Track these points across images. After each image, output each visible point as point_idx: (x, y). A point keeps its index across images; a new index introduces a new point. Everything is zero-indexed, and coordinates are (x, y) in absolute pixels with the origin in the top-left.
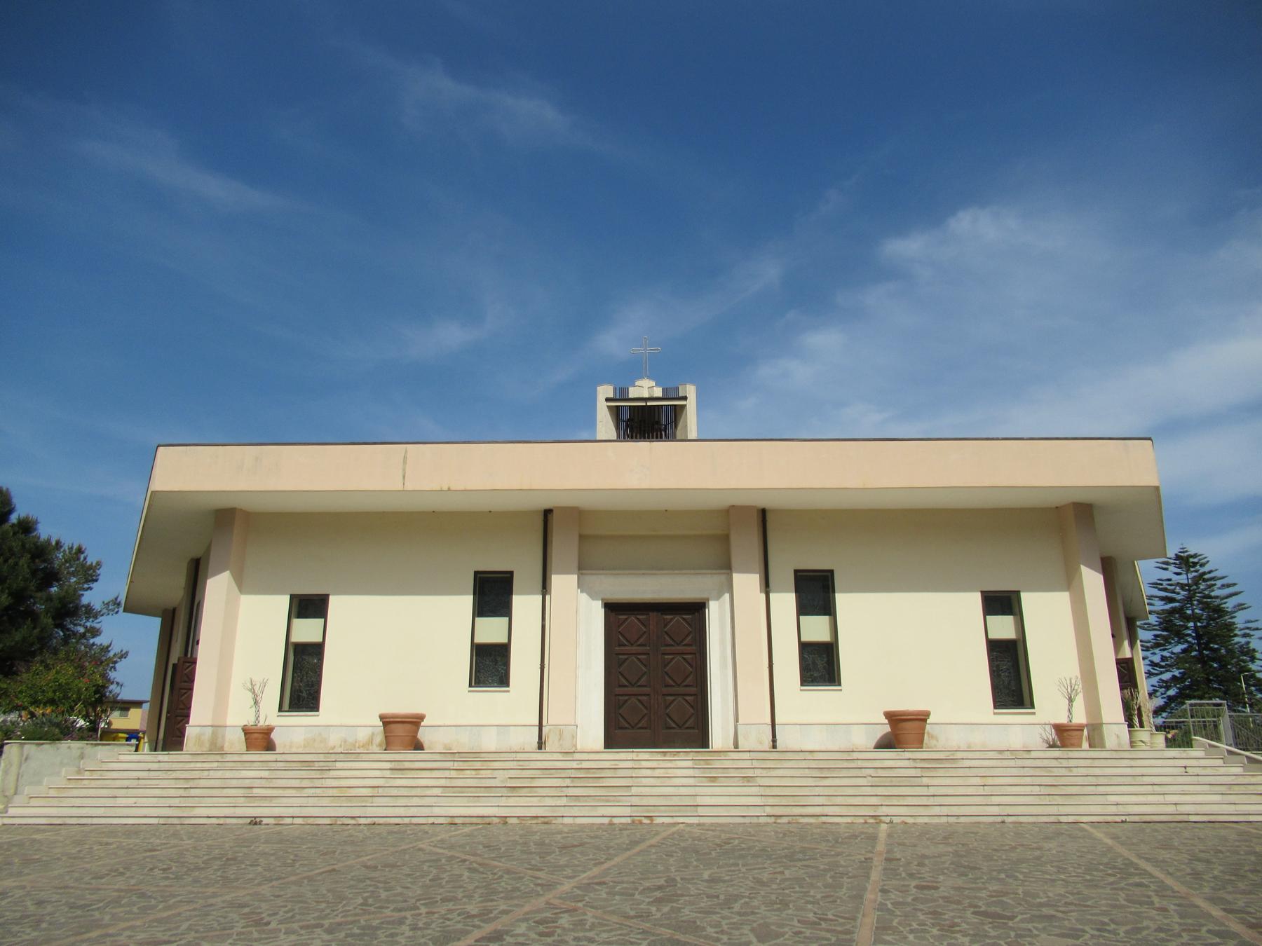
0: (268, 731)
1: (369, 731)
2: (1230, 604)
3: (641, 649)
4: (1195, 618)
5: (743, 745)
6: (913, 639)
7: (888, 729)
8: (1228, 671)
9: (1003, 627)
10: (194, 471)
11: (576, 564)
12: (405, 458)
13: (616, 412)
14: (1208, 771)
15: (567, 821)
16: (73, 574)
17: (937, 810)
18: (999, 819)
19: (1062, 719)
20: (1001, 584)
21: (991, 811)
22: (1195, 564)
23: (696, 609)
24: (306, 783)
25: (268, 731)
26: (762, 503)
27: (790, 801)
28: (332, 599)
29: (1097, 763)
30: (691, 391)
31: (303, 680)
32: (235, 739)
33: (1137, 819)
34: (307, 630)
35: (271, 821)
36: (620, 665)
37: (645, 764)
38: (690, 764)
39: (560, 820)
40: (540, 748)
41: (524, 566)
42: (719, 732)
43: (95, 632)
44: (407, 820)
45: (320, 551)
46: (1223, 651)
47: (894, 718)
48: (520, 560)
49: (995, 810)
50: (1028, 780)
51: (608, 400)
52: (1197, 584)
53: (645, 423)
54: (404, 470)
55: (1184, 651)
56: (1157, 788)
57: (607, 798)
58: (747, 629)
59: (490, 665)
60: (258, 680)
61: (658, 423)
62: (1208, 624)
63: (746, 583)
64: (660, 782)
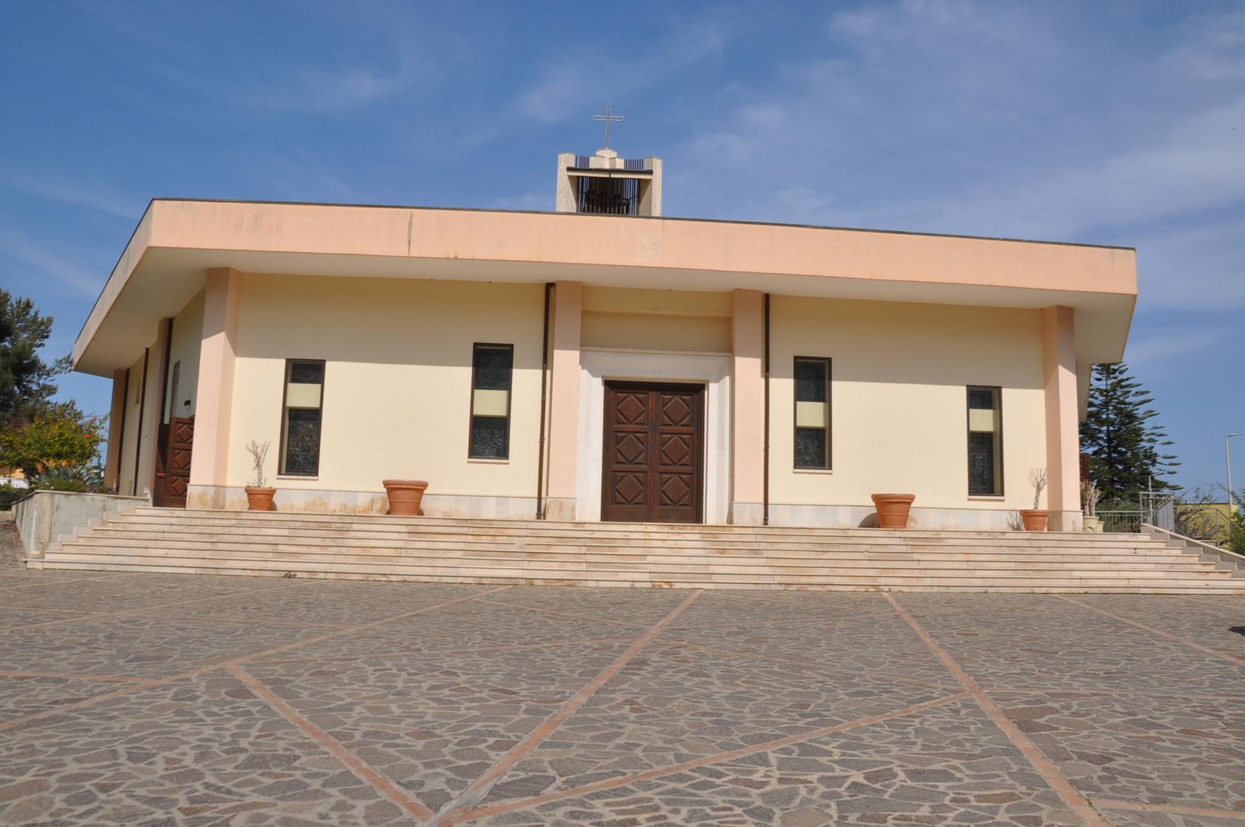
0: (271, 493)
2: (1140, 411)
3: (639, 427)
4: (1109, 422)
5: (737, 521)
6: (901, 428)
7: (874, 511)
9: (983, 420)
10: (187, 228)
11: (579, 340)
12: (410, 224)
13: (577, 183)
14: (1154, 553)
16: (24, 330)
17: (928, 582)
18: (983, 590)
19: (1029, 506)
20: (984, 380)
21: (975, 583)
22: (1115, 371)
23: (696, 391)
27: (796, 571)
28: (328, 364)
29: (1062, 544)
30: (657, 165)
31: (301, 442)
32: (236, 499)
33: (1097, 590)
34: (304, 395)
35: (305, 575)
36: (618, 443)
37: (654, 536)
38: (697, 537)
39: (584, 584)
40: (539, 517)
41: (525, 342)
42: (714, 509)
43: (52, 390)
44: (436, 579)
45: (311, 318)
46: (1129, 454)
47: (882, 501)
48: (519, 332)
50: (1005, 558)
51: (569, 169)
52: (1114, 390)
53: (605, 196)
54: (409, 236)
55: (1095, 453)
57: (625, 566)
58: (746, 409)
59: (489, 437)
60: (259, 442)
61: (620, 196)
62: (1120, 429)
63: (748, 367)
64: (658, 552)
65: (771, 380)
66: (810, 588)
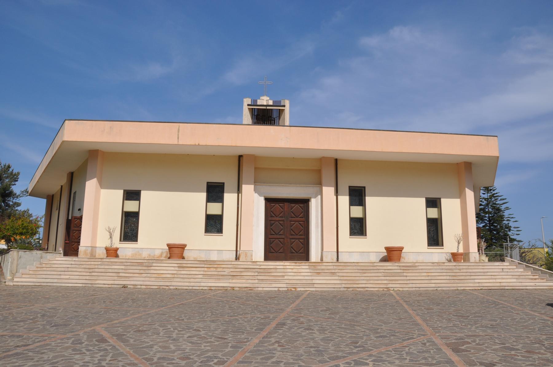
0: (116, 250)
1: (160, 251)
2: (503, 207)
4: (489, 213)
5: (325, 260)
6: (396, 217)
7: (386, 254)
8: (499, 235)
10: (80, 132)
12: (179, 130)
13: (252, 111)
15: (260, 289)
16: (7, 178)
17: (411, 285)
18: (435, 289)
19: (455, 251)
21: (432, 286)
22: (491, 190)
23: (306, 202)
24: (142, 271)
25: (116, 250)
26: (336, 157)
28: (142, 192)
29: (470, 267)
30: (287, 103)
31: (130, 227)
33: (486, 288)
34: (131, 206)
35: (132, 287)
36: (271, 226)
37: (288, 267)
38: (307, 267)
41: (230, 181)
43: (19, 205)
45: (138, 171)
47: (389, 250)
48: (227, 177)
49: (433, 285)
51: (248, 105)
52: (491, 198)
53: (264, 117)
54: (178, 135)
55: (483, 226)
56: (492, 277)
58: (328, 209)
59: (214, 224)
61: (271, 117)
62: (494, 215)
63: (328, 191)
64: (290, 274)
65: (339, 197)
66: (358, 289)
